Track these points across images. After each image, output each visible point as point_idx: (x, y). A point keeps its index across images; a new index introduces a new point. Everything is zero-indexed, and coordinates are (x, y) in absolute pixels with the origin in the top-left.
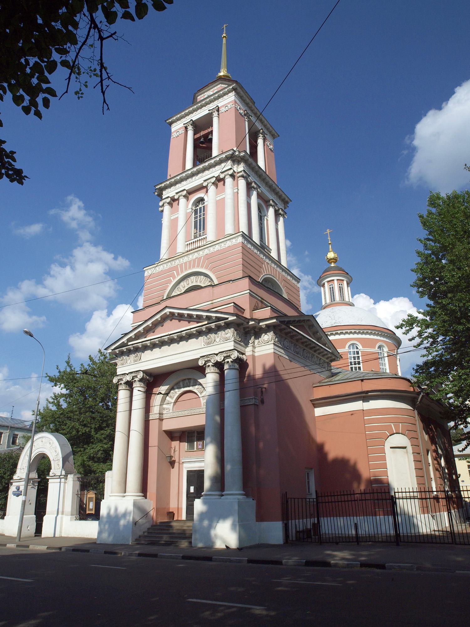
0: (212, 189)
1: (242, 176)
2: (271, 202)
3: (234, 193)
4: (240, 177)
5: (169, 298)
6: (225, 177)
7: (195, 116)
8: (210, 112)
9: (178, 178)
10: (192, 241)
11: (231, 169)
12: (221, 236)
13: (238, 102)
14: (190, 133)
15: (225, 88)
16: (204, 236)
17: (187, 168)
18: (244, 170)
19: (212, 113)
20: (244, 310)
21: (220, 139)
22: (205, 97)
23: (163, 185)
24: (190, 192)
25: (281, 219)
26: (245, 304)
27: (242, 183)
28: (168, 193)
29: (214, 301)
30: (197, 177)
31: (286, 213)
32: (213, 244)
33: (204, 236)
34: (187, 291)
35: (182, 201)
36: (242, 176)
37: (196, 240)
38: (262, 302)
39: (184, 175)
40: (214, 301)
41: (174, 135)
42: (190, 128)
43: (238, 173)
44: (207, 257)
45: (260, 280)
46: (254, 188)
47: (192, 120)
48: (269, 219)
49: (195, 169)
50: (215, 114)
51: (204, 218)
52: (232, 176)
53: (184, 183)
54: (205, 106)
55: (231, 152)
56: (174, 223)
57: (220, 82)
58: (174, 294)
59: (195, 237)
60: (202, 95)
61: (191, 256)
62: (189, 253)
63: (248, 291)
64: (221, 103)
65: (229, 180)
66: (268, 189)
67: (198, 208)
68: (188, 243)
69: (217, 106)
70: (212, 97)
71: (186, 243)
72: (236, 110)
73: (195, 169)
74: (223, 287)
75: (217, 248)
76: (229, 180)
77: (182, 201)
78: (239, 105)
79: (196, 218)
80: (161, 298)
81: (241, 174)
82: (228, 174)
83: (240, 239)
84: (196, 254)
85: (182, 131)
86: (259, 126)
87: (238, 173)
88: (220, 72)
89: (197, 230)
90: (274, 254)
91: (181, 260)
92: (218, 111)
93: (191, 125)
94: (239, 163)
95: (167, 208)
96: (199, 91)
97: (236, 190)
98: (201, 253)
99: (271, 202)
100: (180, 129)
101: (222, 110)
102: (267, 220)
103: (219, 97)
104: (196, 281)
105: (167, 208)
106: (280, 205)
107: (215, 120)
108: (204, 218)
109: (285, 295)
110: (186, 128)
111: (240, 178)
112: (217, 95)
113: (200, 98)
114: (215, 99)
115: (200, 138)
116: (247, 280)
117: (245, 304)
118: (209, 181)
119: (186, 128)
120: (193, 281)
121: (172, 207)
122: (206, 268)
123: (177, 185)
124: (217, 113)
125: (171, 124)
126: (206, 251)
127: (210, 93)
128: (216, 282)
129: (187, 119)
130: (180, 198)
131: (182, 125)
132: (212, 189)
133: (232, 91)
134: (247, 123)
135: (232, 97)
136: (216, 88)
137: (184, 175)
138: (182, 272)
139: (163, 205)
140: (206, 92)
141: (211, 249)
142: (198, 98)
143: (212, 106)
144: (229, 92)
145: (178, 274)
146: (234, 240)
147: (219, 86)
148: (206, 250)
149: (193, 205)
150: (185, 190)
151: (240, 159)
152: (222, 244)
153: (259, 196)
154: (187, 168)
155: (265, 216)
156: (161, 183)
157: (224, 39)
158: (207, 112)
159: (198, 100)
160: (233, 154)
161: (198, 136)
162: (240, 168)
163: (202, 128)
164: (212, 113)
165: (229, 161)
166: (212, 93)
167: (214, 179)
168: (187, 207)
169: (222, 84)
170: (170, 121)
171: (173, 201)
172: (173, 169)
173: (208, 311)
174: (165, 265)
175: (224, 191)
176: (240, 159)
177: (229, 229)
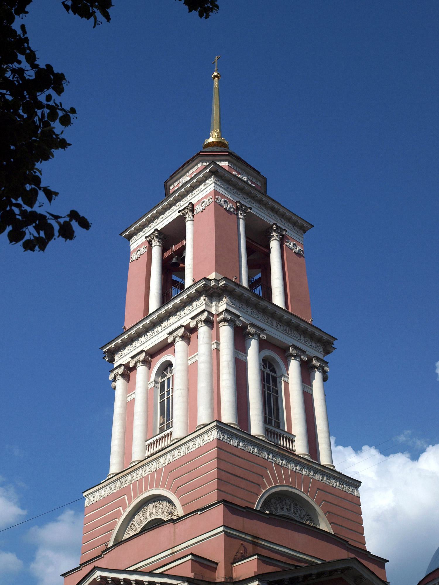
0: (180, 345)
1: (225, 320)
2: (292, 350)
3: (211, 351)
4: (221, 321)
5: (118, 543)
6: (197, 325)
7: (161, 223)
8: (148, 239)
9: (140, 326)
10: (157, 437)
11: (204, 311)
12: (195, 430)
13: (221, 191)
14: (156, 251)
15: (206, 167)
16: (168, 431)
17: (151, 311)
18: (227, 310)
19: (184, 215)
20: (217, 564)
21: (195, 258)
22: (180, 185)
23: (112, 345)
24: (152, 354)
25: (318, 375)
26: (216, 552)
27: (226, 332)
28: (123, 358)
29: (175, 549)
30: (160, 328)
31: (326, 363)
32: (179, 443)
33: (168, 431)
34: (145, 530)
35: (141, 369)
36: (225, 320)
37: (163, 434)
38: (255, 544)
39: (148, 321)
40: (175, 549)
41: (134, 256)
42: (155, 242)
43: (219, 315)
44: (171, 467)
45: (257, 506)
46: (252, 335)
47: (156, 230)
48: (290, 381)
49: (163, 311)
50: (189, 216)
51: (168, 399)
52: (208, 322)
53: (143, 339)
54: (174, 204)
55: (202, 284)
56: (129, 407)
57: (199, 159)
58: (126, 536)
59: (162, 430)
60: (176, 183)
61: (147, 468)
62: (145, 462)
63: (222, 529)
64: (195, 197)
65: (203, 330)
66: (284, 328)
67: (165, 378)
68: (149, 442)
69: (191, 203)
70: (183, 190)
71: (147, 443)
72: (218, 205)
73: (163, 311)
74: (188, 521)
75: (183, 450)
76: (203, 330)
77: (141, 369)
78: (223, 196)
79: (162, 396)
80: (103, 547)
81: (222, 317)
82: (201, 321)
83: (214, 434)
84: (155, 463)
85: (144, 249)
86: (269, 219)
87: (219, 315)
88: (208, 138)
89: (164, 417)
90: (300, 447)
91: (134, 474)
92: (192, 210)
93: (157, 237)
94: (219, 300)
95: (120, 384)
96: (172, 177)
97: (214, 346)
98: (161, 460)
99: (292, 350)
100: (141, 246)
101: (198, 208)
102: (287, 383)
103: (193, 188)
104: (157, 512)
105: (120, 384)
106: (313, 351)
107: (189, 226)
108: (168, 399)
109: (324, 526)
110: (150, 243)
111: (221, 324)
112: (188, 186)
113: (173, 188)
114: (188, 192)
115: (171, 257)
116: (220, 508)
117: (216, 552)
118: (175, 334)
119: (150, 243)
120: (154, 512)
121: (128, 381)
122: (169, 488)
123: (194, 304)
124: (191, 214)
125: (129, 238)
126: (169, 458)
127: (187, 178)
128: (180, 512)
129: (149, 230)
130: (138, 365)
131: (143, 239)
132: (180, 345)
133: (210, 177)
134: (241, 222)
135: (209, 187)
136: (194, 169)
137: (148, 321)
138: (136, 496)
139: (115, 378)
140: (181, 177)
141: (175, 453)
142: (171, 187)
143: (183, 204)
144: (206, 178)
145: (130, 501)
146: (206, 436)
147: (199, 166)
148: (169, 456)
149: (157, 374)
150: (142, 351)
151: (220, 291)
152: (190, 445)
153: (262, 345)
154: (151, 310)
155: (282, 376)
156: (110, 343)
157: (216, 80)
158: (177, 214)
159: (171, 192)
160: (206, 286)
161: (167, 254)
162: (221, 307)
163: (172, 238)
164: (184, 215)
165: (203, 298)
166: (188, 178)
167: (183, 329)
168: (149, 379)
169: (203, 161)
170: (127, 233)
171: (128, 372)
172: (132, 317)
173: (150, 574)
174: (113, 486)
175: (196, 350)
176: (220, 291)
177: (203, 416)
